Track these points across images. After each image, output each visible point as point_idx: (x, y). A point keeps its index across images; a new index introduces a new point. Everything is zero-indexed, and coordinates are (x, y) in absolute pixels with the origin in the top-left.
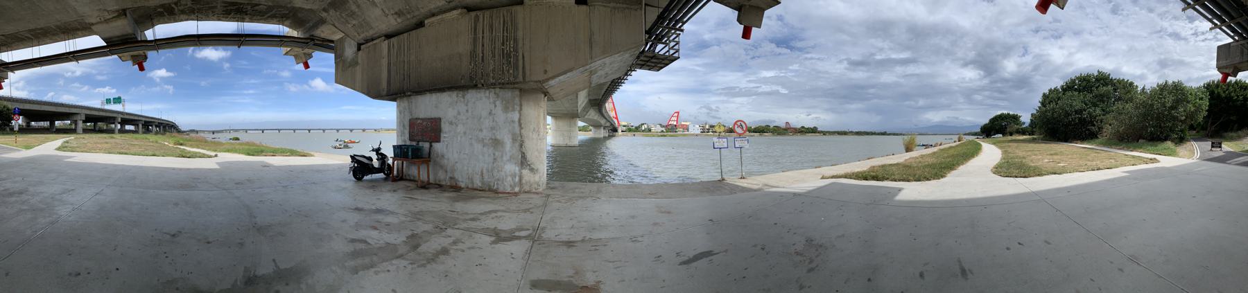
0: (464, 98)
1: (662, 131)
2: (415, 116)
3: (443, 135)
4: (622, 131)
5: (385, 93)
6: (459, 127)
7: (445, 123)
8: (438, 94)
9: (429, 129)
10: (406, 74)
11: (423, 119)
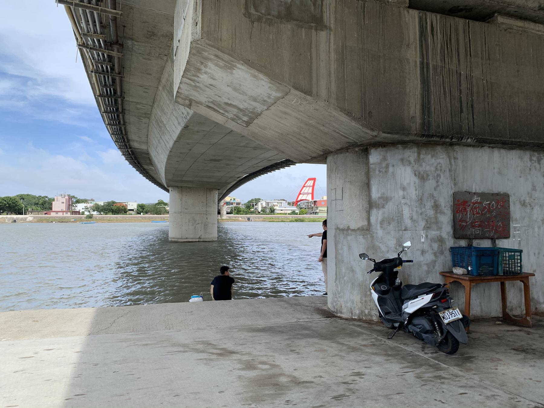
0: (539, 164)
1: (294, 213)
2: (465, 188)
3: (513, 225)
4: (227, 213)
5: (416, 125)
6: (535, 211)
7: (514, 204)
8: (503, 151)
9: (494, 214)
10: (464, 98)
11: (483, 195)
